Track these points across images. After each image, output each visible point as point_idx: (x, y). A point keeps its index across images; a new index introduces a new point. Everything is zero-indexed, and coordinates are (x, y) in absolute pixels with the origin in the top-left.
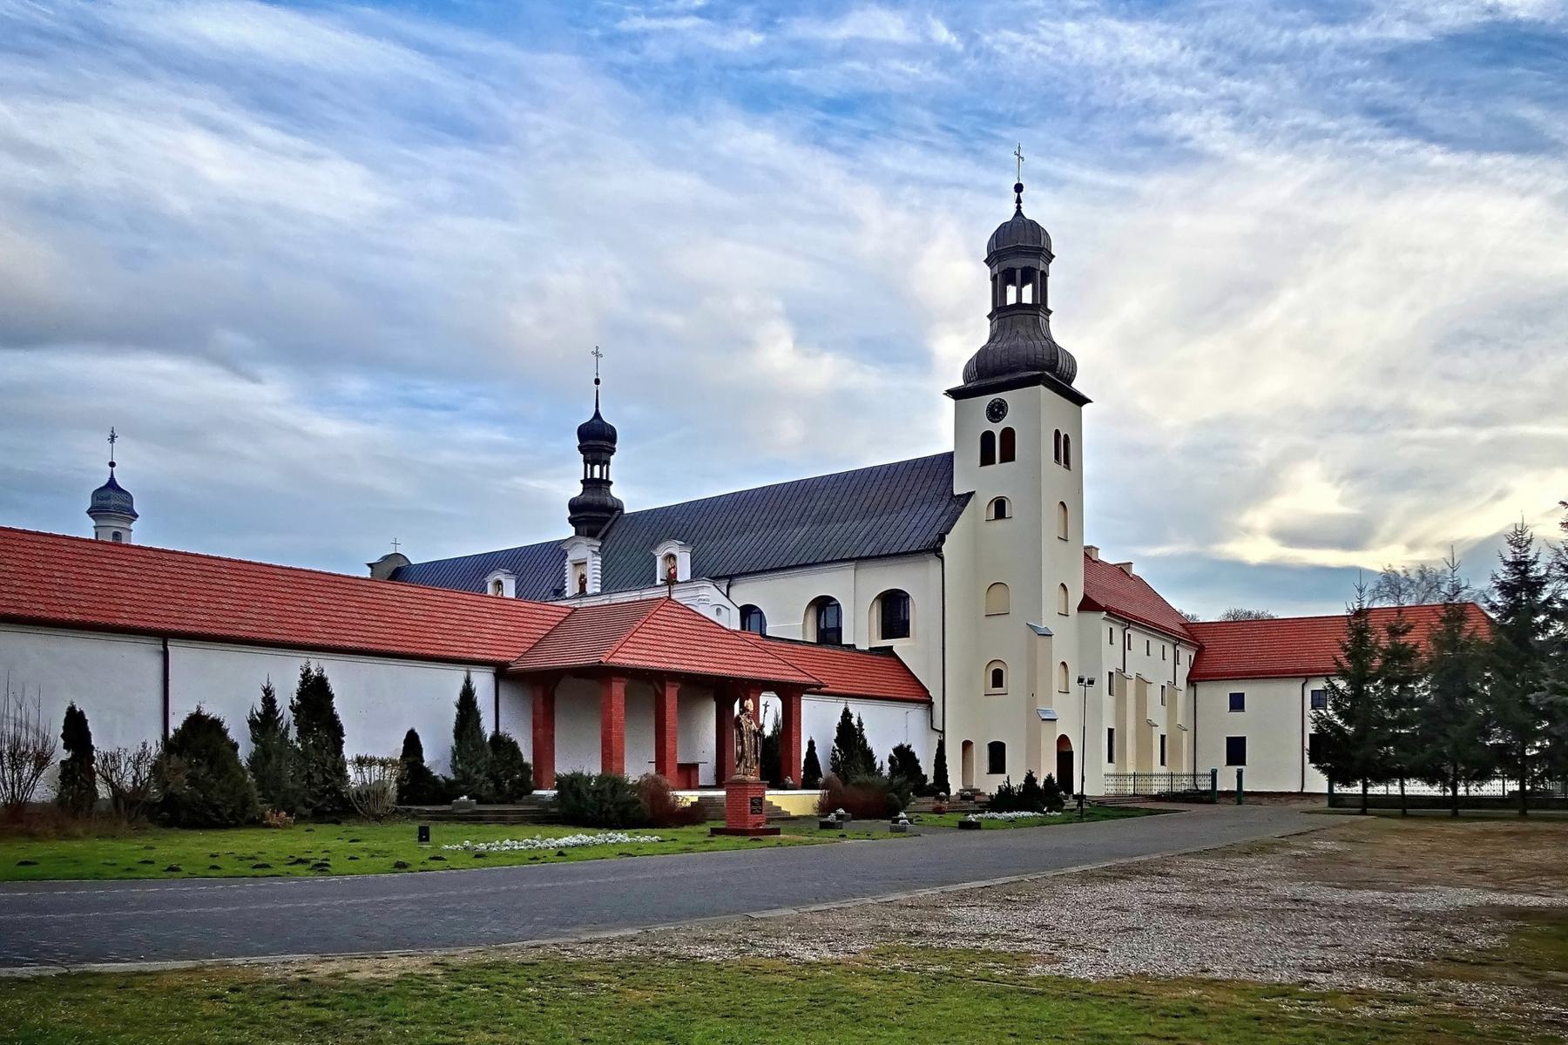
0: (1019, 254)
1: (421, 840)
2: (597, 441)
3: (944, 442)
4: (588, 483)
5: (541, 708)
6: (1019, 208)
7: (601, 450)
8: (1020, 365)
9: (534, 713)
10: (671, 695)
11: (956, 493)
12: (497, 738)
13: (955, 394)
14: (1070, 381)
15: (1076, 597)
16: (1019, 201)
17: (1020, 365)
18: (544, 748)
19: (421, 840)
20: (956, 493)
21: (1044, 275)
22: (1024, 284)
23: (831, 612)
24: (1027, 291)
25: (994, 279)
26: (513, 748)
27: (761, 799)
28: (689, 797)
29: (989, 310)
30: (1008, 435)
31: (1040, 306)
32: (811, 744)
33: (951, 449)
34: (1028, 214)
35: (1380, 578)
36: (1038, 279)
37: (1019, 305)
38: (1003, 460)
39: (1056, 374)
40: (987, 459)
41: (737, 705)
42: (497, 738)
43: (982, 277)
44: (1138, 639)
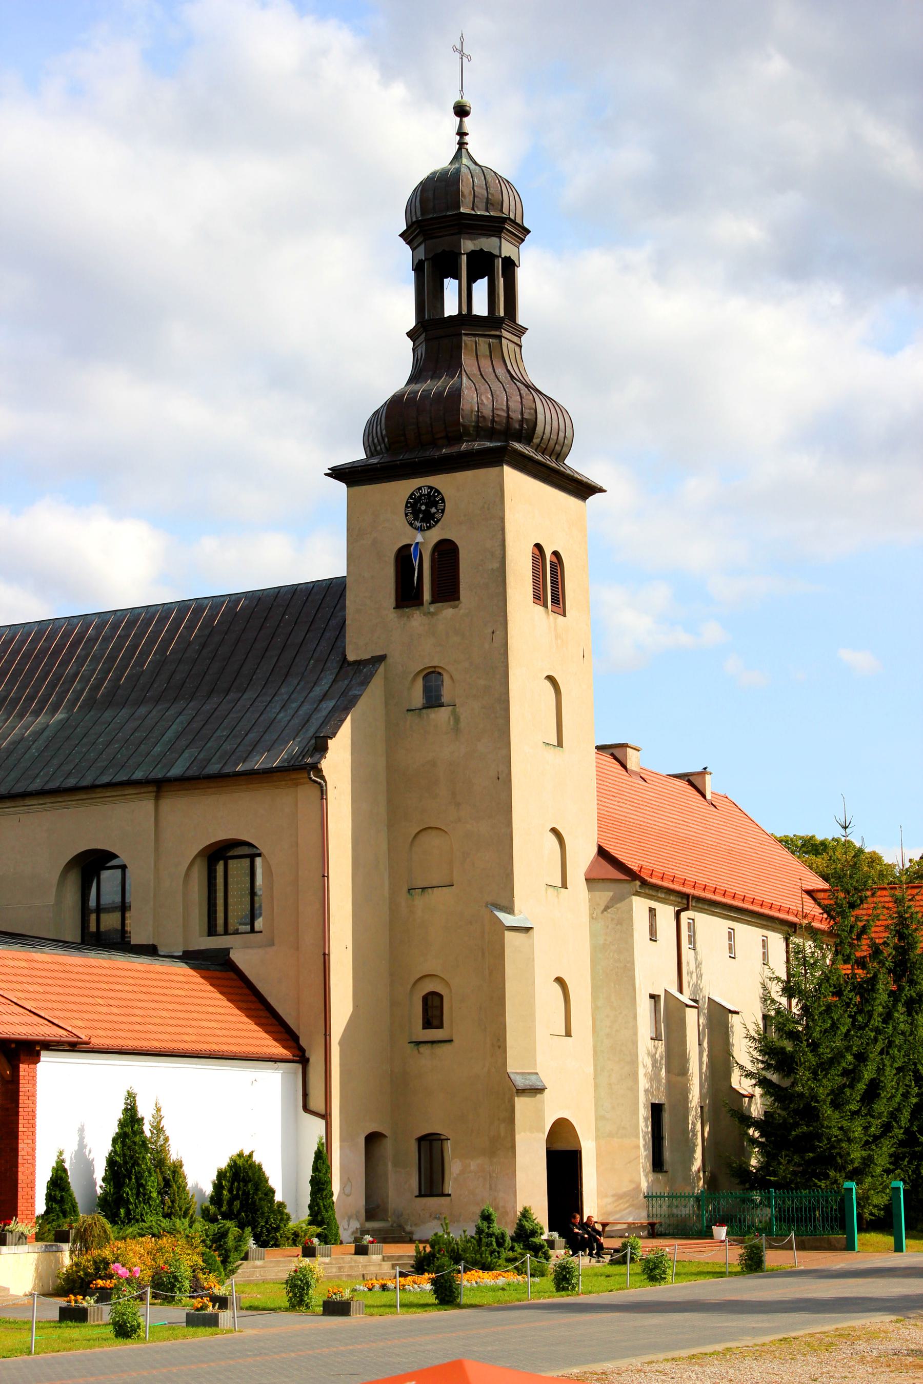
0: (457, 231)
3: (319, 556)
6: (462, 144)
8: (452, 432)
11: (351, 657)
14: (560, 456)
15: (582, 855)
16: (462, 134)
17: (452, 432)
20: (351, 657)
21: (510, 266)
22: (472, 279)
23: (109, 878)
24: (481, 288)
25: (418, 268)
29: (411, 323)
30: (447, 552)
31: (503, 320)
33: (343, 573)
34: (458, 119)
37: (466, 319)
38: (433, 602)
39: (531, 444)
40: (407, 595)
41: (122, 1211)
44: (710, 927)
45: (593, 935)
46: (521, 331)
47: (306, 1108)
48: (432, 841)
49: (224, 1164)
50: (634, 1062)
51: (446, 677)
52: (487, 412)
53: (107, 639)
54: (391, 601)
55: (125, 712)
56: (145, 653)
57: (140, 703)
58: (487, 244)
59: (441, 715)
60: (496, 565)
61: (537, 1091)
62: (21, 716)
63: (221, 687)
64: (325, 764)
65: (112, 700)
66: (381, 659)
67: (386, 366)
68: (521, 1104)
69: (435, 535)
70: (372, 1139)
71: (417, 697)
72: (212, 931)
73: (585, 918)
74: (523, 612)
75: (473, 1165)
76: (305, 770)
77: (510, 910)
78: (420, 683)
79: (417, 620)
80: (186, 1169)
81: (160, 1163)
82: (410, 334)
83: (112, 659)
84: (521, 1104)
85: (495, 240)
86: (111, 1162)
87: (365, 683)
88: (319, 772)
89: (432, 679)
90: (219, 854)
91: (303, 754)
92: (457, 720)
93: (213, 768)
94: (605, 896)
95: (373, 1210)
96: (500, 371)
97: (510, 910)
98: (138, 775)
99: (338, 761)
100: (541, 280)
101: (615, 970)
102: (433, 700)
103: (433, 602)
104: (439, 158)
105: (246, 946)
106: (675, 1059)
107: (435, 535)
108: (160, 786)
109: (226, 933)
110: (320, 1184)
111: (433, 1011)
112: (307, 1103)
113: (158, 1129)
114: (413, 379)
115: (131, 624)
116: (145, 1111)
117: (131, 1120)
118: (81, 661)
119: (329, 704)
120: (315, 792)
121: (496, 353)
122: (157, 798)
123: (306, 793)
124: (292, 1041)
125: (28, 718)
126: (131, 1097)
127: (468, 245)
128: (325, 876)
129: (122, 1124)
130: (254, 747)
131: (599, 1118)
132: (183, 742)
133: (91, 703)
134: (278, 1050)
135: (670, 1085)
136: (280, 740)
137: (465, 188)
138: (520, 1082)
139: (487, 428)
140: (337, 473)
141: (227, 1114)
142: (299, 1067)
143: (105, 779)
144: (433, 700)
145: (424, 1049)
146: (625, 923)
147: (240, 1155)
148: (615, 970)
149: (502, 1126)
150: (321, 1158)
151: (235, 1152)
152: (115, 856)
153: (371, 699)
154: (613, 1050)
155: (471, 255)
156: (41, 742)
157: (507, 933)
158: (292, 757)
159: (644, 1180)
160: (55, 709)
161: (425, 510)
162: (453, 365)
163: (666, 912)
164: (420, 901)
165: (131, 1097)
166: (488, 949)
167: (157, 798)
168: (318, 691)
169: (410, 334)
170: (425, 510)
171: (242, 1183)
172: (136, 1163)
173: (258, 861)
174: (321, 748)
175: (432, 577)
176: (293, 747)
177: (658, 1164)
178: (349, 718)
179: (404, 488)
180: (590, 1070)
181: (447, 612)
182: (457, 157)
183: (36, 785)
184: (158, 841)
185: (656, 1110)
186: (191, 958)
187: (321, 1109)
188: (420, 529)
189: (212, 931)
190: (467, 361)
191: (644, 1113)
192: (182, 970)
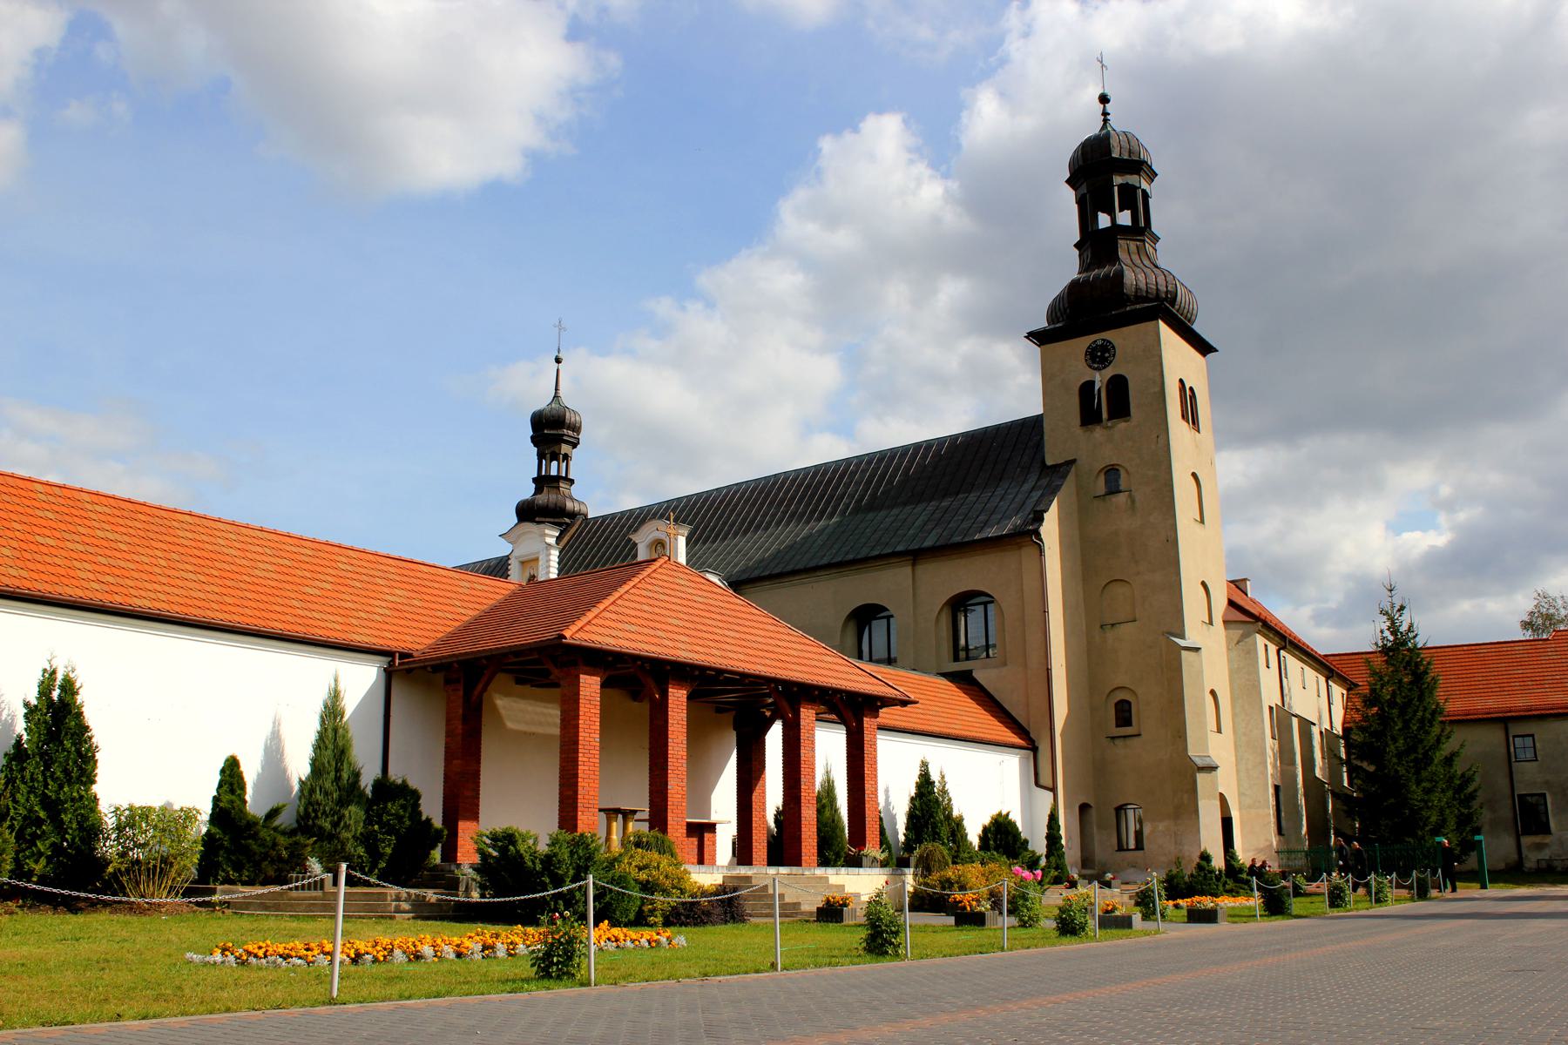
1: (1333, 905)
2: (552, 432)
4: (542, 482)
5: (459, 727)
7: (560, 440)
9: (449, 734)
10: (678, 697)
11: (1049, 462)
12: (385, 788)
13: (1038, 337)
16: (1105, 114)
18: (462, 797)
19: (1333, 905)
20: (1049, 462)
25: (1081, 202)
26: (409, 796)
27: (908, 866)
28: (706, 878)
30: (1118, 386)
31: (1141, 230)
32: (887, 791)
33: (1040, 411)
35: (1379, 661)
36: (1134, 199)
37: (1116, 229)
38: (1110, 418)
40: (1089, 417)
42: (385, 788)
43: (1067, 200)
44: (1293, 663)
45: (1229, 661)
46: (1156, 239)
47: (1037, 784)
48: (1119, 590)
49: (987, 821)
50: (1264, 753)
51: (1122, 472)
52: (1143, 285)
53: (864, 471)
54: (1078, 421)
55: (883, 513)
56: (893, 476)
57: (891, 507)
58: (1132, 179)
59: (1121, 498)
60: (1157, 389)
61: (1213, 768)
62: (808, 522)
63: (955, 495)
64: (1043, 530)
65: (873, 506)
66: (1073, 462)
67: (1066, 268)
68: (1201, 778)
69: (1109, 372)
70: (1084, 808)
71: (1101, 486)
72: (956, 659)
73: (1224, 649)
74: (1177, 427)
75: (1161, 826)
76: (1028, 535)
77: (1182, 637)
78: (1102, 477)
79: (1098, 433)
80: (965, 823)
81: (949, 817)
82: (1076, 246)
83: (869, 482)
84: (1201, 778)
85: (1136, 177)
86: (911, 816)
87: (1064, 477)
88: (1038, 535)
89: (1112, 473)
90: (960, 604)
91: (1025, 523)
92: (1133, 502)
93: (957, 539)
94: (1237, 633)
95: (1086, 862)
96: (1147, 262)
97: (1182, 637)
98: (900, 548)
99: (1050, 529)
100: (1168, 207)
101: (1246, 687)
102: (1113, 489)
103: (1110, 418)
104: (1094, 129)
105: (984, 668)
106: (1285, 754)
107: (1109, 372)
108: (916, 556)
109: (968, 658)
110: (1053, 838)
111: (1124, 714)
112: (1038, 779)
113: (944, 792)
114: (1084, 268)
115: (880, 460)
116: (935, 777)
117: (925, 783)
118: (847, 486)
119: (1036, 495)
120: (1034, 551)
121: (1140, 251)
122: (914, 565)
123: (1028, 553)
124: (1023, 732)
125: (812, 523)
126: (924, 765)
127: (1118, 180)
128: (1045, 612)
129: (919, 786)
130: (986, 524)
131: (1241, 794)
132: (929, 526)
133: (857, 510)
134: (1017, 740)
135: (1283, 773)
136: (1006, 517)
137: (1114, 142)
138: (1199, 762)
139: (1140, 297)
140: (1032, 336)
141: (986, 785)
142: (1031, 754)
143: (876, 553)
144: (1113, 489)
145: (1117, 742)
146: (1252, 652)
147: (1000, 814)
148: (1246, 687)
149: (1186, 796)
150: (1053, 818)
151: (995, 812)
152: (886, 609)
153: (1068, 487)
154: (1246, 745)
155: (1120, 186)
156: (824, 537)
157: (1184, 653)
158: (1016, 527)
159: (1274, 840)
160: (831, 516)
161: (1100, 356)
162: (1113, 258)
163: (1273, 648)
164: (1110, 635)
165: (924, 765)
166: (1169, 664)
167: (914, 565)
168: (1027, 487)
169: (1076, 246)
170: (1100, 356)
171: (1001, 835)
172: (932, 816)
173: (990, 607)
174: (1039, 518)
175: (1111, 402)
176: (1016, 521)
177: (1280, 831)
178: (1054, 507)
179: (1085, 342)
180: (1233, 759)
181: (1122, 425)
182: (1104, 126)
183: (825, 561)
184: (914, 594)
185: (1277, 788)
186: (952, 677)
187: (1050, 785)
188: (1098, 369)
189: (956, 659)
190: (1122, 255)
191: (1271, 791)
192: (943, 682)
